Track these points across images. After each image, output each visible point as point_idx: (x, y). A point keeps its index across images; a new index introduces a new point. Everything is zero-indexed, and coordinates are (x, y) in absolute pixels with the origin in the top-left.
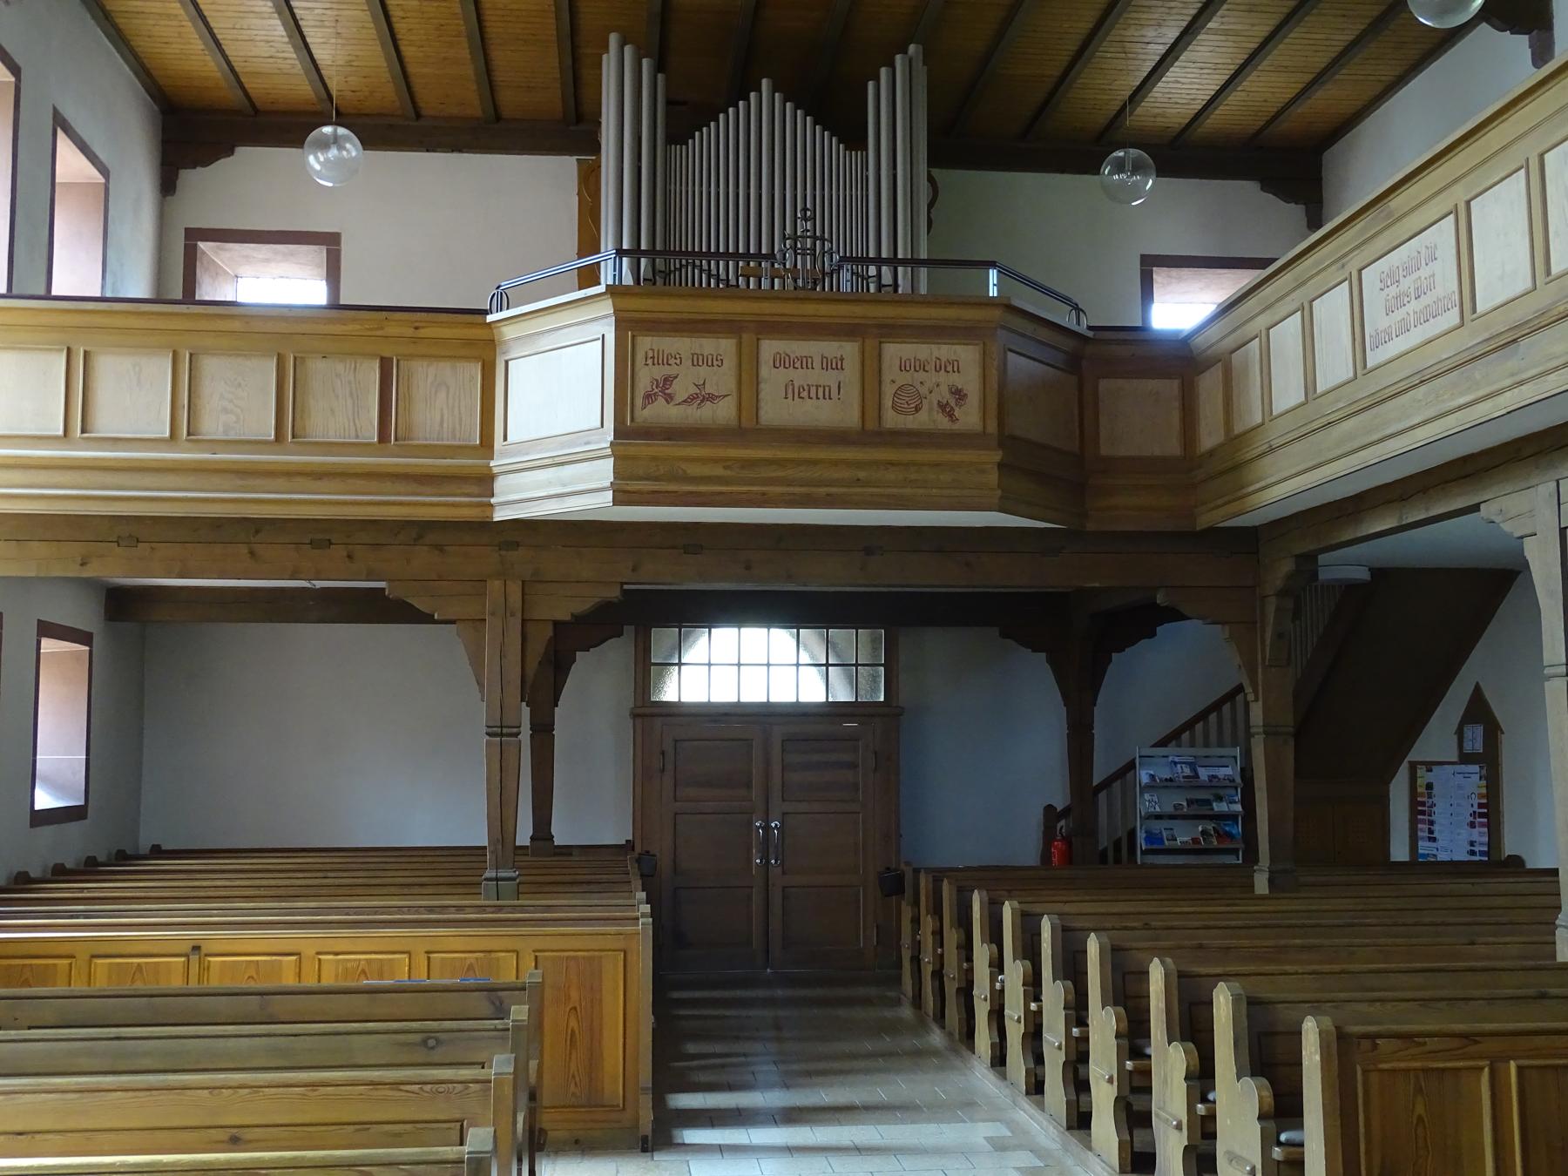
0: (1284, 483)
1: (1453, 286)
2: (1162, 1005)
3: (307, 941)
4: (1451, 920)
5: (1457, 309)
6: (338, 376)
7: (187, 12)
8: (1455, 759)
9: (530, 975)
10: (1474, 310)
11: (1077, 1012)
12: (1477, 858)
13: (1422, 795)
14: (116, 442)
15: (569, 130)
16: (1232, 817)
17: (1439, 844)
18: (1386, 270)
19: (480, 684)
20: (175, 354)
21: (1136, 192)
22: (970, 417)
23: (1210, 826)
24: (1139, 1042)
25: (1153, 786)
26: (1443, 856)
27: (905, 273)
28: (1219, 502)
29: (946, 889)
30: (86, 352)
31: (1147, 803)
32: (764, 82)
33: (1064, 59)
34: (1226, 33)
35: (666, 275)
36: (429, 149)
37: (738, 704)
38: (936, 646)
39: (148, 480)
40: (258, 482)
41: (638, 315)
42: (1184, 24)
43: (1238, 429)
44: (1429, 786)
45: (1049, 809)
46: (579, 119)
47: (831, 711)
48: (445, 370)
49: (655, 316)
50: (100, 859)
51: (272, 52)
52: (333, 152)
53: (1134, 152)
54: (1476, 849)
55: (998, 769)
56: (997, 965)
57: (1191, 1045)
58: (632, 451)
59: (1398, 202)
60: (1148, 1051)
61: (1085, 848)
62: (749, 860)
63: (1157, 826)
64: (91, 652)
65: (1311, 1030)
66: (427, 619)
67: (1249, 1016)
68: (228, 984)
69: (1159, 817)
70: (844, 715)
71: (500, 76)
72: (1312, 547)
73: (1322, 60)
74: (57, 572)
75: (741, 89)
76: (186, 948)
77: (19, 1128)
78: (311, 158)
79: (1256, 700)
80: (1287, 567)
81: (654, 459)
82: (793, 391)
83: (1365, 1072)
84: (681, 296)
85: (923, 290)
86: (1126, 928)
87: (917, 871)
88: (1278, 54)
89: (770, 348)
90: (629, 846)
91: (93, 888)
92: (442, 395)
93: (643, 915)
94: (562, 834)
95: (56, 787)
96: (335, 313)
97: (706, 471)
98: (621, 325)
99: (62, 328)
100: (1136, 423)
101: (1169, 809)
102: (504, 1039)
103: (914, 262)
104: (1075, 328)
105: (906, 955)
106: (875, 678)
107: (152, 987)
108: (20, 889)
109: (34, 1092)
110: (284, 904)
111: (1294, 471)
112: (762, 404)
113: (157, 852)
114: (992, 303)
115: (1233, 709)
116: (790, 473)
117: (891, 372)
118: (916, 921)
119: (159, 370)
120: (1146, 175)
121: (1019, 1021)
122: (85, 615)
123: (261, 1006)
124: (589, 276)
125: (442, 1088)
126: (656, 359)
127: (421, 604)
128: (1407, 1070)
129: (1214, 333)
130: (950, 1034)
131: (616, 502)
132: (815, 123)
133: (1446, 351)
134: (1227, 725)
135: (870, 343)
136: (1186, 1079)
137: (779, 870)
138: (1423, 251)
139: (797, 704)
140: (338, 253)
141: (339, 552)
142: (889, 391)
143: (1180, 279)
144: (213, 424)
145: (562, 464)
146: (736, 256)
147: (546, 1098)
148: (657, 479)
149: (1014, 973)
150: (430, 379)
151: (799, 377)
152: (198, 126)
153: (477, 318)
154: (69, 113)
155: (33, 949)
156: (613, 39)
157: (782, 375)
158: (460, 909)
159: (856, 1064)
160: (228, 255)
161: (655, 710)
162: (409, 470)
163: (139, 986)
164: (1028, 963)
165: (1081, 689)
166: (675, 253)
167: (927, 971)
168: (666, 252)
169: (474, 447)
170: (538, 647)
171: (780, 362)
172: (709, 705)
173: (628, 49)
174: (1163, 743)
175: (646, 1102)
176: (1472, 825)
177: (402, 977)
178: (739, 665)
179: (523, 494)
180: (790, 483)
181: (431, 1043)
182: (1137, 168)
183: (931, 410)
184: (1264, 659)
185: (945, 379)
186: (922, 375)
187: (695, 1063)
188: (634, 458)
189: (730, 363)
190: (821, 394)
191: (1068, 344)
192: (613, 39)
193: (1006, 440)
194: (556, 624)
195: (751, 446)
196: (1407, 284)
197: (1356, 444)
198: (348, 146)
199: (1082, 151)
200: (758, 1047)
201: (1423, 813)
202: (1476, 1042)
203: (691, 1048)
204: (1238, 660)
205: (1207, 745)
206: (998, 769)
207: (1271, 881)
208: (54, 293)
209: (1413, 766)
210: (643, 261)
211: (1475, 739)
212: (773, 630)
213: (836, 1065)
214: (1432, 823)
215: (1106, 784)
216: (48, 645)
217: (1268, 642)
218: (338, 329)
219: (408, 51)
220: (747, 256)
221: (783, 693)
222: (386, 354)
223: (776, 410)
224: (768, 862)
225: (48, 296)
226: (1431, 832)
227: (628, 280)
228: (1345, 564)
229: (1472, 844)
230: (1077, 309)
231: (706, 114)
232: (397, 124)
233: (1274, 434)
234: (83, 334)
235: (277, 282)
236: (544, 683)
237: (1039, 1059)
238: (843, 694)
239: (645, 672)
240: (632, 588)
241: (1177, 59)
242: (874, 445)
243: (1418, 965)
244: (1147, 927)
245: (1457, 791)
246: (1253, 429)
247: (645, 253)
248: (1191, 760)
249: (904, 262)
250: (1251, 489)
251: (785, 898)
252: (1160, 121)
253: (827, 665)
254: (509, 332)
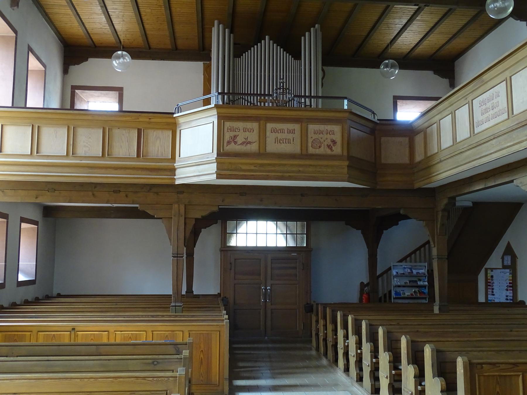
0: (445, 173)
1: (506, 105)
2: (406, 352)
3: (111, 327)
4: (503, 323)
5: (507, 113)
6: (123, 135)
7: (73, 13)
9: (187, 340)
11: (375, 353)
12: (509, 301)
13: (489, 279)
14: (48, 157)
15: (200, 53)
16: (425, 287)
18: (481, 100)
19: (170, 240)
20: (68, 127)
22: (338, 150)
23: (417, 290)
25: (397, 276)
27: (314, 102)
31: (395, 282)
32: (267, 37)
34: (423, 21)
35: (234, 102)
36: (154, 59)
37: (256, 247)
38: (323, 228)
39: (60, 169)
42: (409, 18)
44: (492, 277)
45: (362, 283)
46: (204, 49)
47: (287, 250)
48: (159, 133)
49: (230, 115)
50: (40, 298)
51: (101, 26)
52: (121, 60)
53: (391, 61)
54: (508, 298)
55: (344, 270)
56: (346, 337)
57: (416, 366)
59: (485, 77)
60: (400, 367)
61: (374, 297)
62: (260, 300)
63: (398, 290)
65: (460, 361)
66: (152, 217)
68: (84, 342)
69: (399, 286)
70: (292, 251)
71: (177, 35)
72: (455, 195)
75: (259, 39)
76: (70, 329)
77: (14, 392)
78: (114, 62)
79: (435, 247)
80: (445, 201)
81: (230, 163)
82: (278, 141)
83: (479, 376)
84: (286, 110)
85: (320, 106)
86: (391, 325)
87: (317, 304)
90: (219, 295)
91: (38, 308)
92: (158, 142)
93: (226, 319)
95: (26, 273)
98: (221, 118)
100: (394, 152)
101: (403, 284)
103: (317, 97)
104: (373, 120)
105: (314, 333)
106: (303, 238)
107: (57, 343)
108: (14, 308)
109: (20, 379)
110: (103, 314)
111: (449, 168)
112: (267, 145)
113: (59, 296)
114: (345, 111)
116: (277, 168)
117: (311, 134)
118: (317, 322)
119: (63, 132)
120: (396, 69)
121: (354, 356)
122: (36, 215)
123: (96, 350)
124: (207, 102)
125: (160, 379)
126: (231, 129)
127: (151, 212)
128: (494, 376)
129: (420, 122)
130: (329, 360)
131: (217, 178)
132: (284, 51)
133: (503, 128)
134: (422, 255)
136: (414, 377)
137: (270, 304)
138: (495, 93)
139: (276, 247)
142: (310, 141)
143: (406, 104)
144: (81, 151)
145: (199, 165)
146: (257, 95)
147: (194, 381)
149: (352, 340)
151: (280, 136)
152: (76, 51)
153: (170, 115)
154: (33, 46)
155: (13, 329)
156: (216, 22)
157: (274, 135)
158: (163, 316)
159: (297, 371)
161: (230, 249)
162: (147, 167)
163: (54, 342)
165: (373, 243)
168: (234, 94)
169: (169, 159)
170: (190, 227)
171: (273, 131)
172: (247, 247)
173: (221, 26)
174: (401, 261)
175: (227, 383)
176: (507, 290)
178: (257, 234)
179: (185, 175)
181: (155, 363)
182: (393, 66)
183: (324, 147)
185: (329, 137)
187: (242, 370)
188: (224, 163)
189: (256, 131)
191: (371, 125)
192: (216, 22)
193: (350, 158)
195: (264, 159)
196: (489, 105)
197: (471, 160)
199: (374, 61)
200: (263, 364)
201: (490, 286)
202: (518, 366)
203: (241, 364)
204: (428, 233)
205: (416, 262)
206: (344, 270)
207: (440, 309)
209: (486, 270)
210: (226, 96)
211: (508, 260)
212: (268, 222)
213: (291, 371)
214: (493, 289)
215: (382, 275)
216: (24, 225)
219: (147, 26)
220: (261, 95)
221: (271, 243)
222: (140, 127)
223: (272, 147)
224: (266, 301)
226: (493, 292)
227: (221, 103)
228: (464, 201)
229: (507, 296)
232: (143, 51)
233: (442, 156)
235: (102, 103)
236: (191, 240)
237: (361, 369)
238: (291, 244)
239: (225, 236)
240: (222, 207)
242: (305, 159)
243: (495, 339)
244: (398, 324)
245: (502, 278)
246: (434, 154)
247: (226, 94)
248: (410, 267)
249: (314, 97)
250: (434, 175)
251: (272, 313)
252: (400, 51)
253: (287, 234)
254: (181, 120)
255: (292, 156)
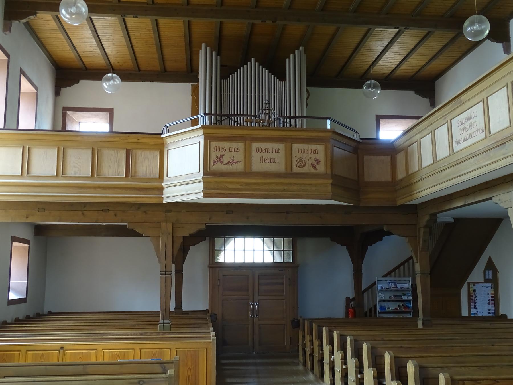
0: (426, 190)
2: (389, 368)
4: (485, 337)
5: (484, 133)
6: (112, 155)
8: (483, 281)
9: (175, 358)
10: (490, 133)
11: (360, 369)
12: (491, 315)
13: (472, 293)
15: (189, 75)
16: (409, 301)
17: (478, 310)
19: (158, 258)
20: (58, 148)
21: (374, 94)
22: (321, 168)
23: (401, 304)
24: (381, 380)
25: (382, 291)
26: (479, 314)
27: (299, 121)
28: (404, 196)
29: (314, 326)
30: (189, 21)
31: (380, 296)
32: (253, 59)
33: (350, 52)
35: (220, 122)
38: (309, 244)
39: (49, 190)
40: (85, 190)
41: (212, 135)
42: (390, 40)
43: (410, 172)
44: (474, 291)
45: (348, 298)
46: (192, 71)
47: (275, 266)
50: (31, 316)
51: (92, 50)
52: (111, 82)
53: (373, 81)
54: (491, 312)
55: (331, 284)
56: (332, 352)
58: (209, 180)
59: (463, 98)
61: (360, 312)
62: (248, 316)
63: (384, 304)
64: (29, 247)
66: (141, 235)
67: (419, 371)
68: (72, 361)
69: (384, 301)
71: (166, 57)
73: (435, 52)
74: (18, 220)
75: (245, 61)
76: (58, 348)
79: (417, 262)
80: (427, 218)
81: (217, 182)
82: (263, 160)
85: (305, 127)
86: (375, 340)
87: (304, 320)
88: (419, 51)
89: (255, 146)
90: (208, 311)
93: (213, 336)
94: (185, 307)
95: (16, 292)
96: (112, 135)
97: (234, 186)
98: (207, 138)
99: (18, 140)
100: (376, 170)
101: (388, 298)
102: (166, 381)
103: (301, 117)
105: (301, 348)
106: (289, 255)
107: (45, 363)
111: (430, 186)
112: (252, 164)
113: (50, 313)
115: (409, 265)
116: (263, 187)
118: (304, 337)
121: (339, 372)
122: (28, 234)
124: (195, 122)
126: (217, 149)
127: (139, 231)
129: (402, 141)
130: (316, 376)
131: (204, 197)
132: (269, 72)
133: (480, 147)
135: (288, 144)
137: (258, 319)
138: (472, 113)
139: (264, 263)
140: (113, 115)
141: (112, 213)
142: (294, 160)
143: (389, 123)
144: (70, 171)
145: (186, 184)
146: (243, 115)
148: (217, 189)
149: (338, 355)
150: (143, 156)
151: (265, 155)
152: (67, 74)
153: (158, 136)
154: (25, 70)
155: (7, 348)
156: (203, 45)
160: (76, 115)
161: (215, 265)
164: (342, 352)
165: (358, 258)
166: (223, 115)
167: (308, 354)
168: (220, 114)
170: (178, 245)
171: (259, 150)
172: (234, 263)
173: (208, 49)
174: (385, 276)
176: (489, 304)
177: (131, 358)
179: (173, 194)
180: (262, 190)
181: (141, 382)
182: (375, 87)
184: (419, 249)
185: (313, 156)
186: (305, 155)
188: (210, 182)
189: (242, 151)
190: (272, 161)
192: (203, 45)
193: (333, 176)
194: (184, 237)
195: (249, 178)
196: (467, 124)
198: (116, 80)
199: (357, 81)
200: (251, 380)
201: (472, 299)
204: (411, 249)
205: (400, 277)
206: (331, 284)
207: (423, 323)
208: (19, 128)
209: (469, 284)
210: (213, 117)
211: (489, 274)
212: (255, 239)
214: (475, 303)
215: (367, 290)
216: (15, 244)
217: (421, 243)
218: (113, 140)
219: (136, 49)
220: (247, 115)
221: (259, 260)
222: (128, 148)
223: (257, 166)
224: (254, 316)
225: (17, 129)
226: (475, 306)
227: (208, 123)
228: (446, 217)
229: (489, 310)
230: (356, 132)
231: (234, 69)
233: (423, 174)
234: (28, 142)
235: (92, 124)
238: (279, 260)
239: (213, 253)
241: (387, 51)
244: (383, 340)
245: (484, 293)
246: (415, 172)
247: (213, 114)
248: (395, 282)
249: (298, 117)
250: (415, 192)
253: (273, 250)
254: (169, 141)
255: (278, 175)
